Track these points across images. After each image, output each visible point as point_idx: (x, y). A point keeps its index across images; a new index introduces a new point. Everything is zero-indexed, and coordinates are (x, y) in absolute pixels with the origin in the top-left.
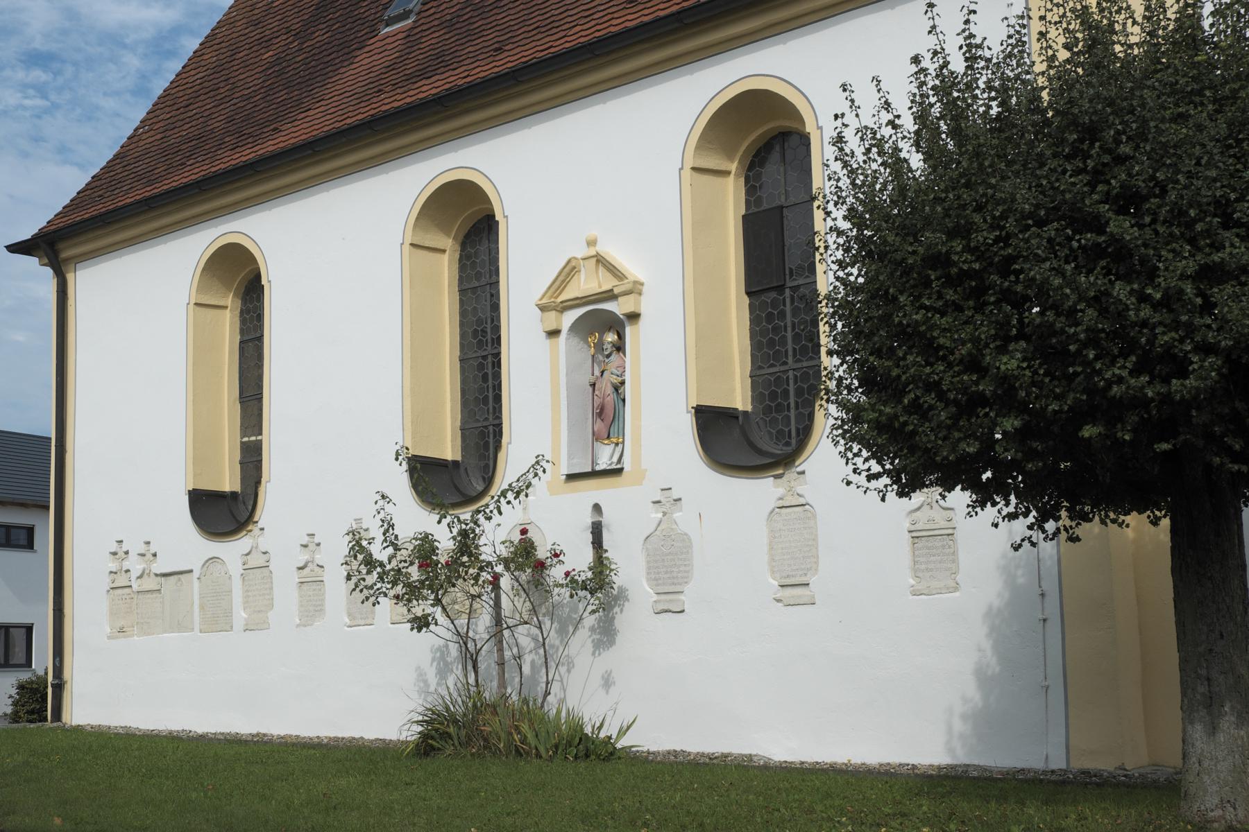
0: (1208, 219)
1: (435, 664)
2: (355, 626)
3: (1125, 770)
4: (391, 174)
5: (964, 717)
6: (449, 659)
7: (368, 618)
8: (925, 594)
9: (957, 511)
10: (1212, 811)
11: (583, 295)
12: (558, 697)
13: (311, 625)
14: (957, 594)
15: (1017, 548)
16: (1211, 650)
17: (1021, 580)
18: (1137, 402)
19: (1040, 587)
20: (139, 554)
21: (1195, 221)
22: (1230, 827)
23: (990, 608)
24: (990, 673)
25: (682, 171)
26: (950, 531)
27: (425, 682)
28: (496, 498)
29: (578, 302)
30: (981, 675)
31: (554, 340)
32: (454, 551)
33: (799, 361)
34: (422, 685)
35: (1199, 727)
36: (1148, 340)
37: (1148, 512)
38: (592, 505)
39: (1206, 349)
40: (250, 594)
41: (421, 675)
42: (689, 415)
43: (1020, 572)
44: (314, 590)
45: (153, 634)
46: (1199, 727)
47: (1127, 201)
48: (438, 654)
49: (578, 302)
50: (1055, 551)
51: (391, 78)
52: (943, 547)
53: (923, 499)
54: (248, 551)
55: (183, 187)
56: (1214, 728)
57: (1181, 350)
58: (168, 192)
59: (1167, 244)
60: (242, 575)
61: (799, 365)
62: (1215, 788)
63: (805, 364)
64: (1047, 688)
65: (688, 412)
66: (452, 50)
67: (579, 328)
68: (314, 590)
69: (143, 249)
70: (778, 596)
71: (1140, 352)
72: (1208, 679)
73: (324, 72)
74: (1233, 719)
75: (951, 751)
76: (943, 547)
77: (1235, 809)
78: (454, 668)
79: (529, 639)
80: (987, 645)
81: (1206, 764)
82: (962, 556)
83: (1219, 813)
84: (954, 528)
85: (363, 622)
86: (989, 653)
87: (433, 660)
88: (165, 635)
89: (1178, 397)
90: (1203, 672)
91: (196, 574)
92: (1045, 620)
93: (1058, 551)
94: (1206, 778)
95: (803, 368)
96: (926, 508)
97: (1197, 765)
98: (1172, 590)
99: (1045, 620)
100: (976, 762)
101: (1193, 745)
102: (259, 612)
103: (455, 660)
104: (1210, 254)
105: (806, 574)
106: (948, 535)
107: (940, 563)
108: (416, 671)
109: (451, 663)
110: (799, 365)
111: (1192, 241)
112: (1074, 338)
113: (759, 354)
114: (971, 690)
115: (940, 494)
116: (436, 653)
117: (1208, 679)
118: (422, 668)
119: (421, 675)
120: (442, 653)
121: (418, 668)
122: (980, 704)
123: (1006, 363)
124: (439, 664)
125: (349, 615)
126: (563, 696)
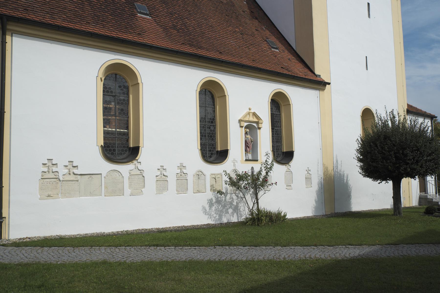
1: (209, 204)
2: (180, 194)
5: (314, 208)
12: (243, 210)
14: (311, 188)
20: (64, 166)
27: (205, 209)
28: (262, 163)
29: (248, 121)
31: (242, 128)
34: (204, 210)
38: (252, 167)
40: (132, 183)
42: (98, 147)
45: (73, 197)
49: (248, 121)
54: (140, 169)
55: (47, 24)
58: (71, 29)
60: (129, 177)
61: (276, 144)
63: (278, 144)
65: (270, 150)
66: (119, 26)
67: (247, 127)
73: (249, 51)
85: (182, 193)
86: (316, 197)
88: (80, 198)
91: (104, 175)
102: (137, 189)
103: (215, 202)
108: (202, 206)
109: (214, 203)
110: (276, 144)
113: (204, 137)
118: (204, 206)
119: (204, 208)
120: (211, 201)
122: (315, 205)
124: (210, 204)
125: (177, 191)
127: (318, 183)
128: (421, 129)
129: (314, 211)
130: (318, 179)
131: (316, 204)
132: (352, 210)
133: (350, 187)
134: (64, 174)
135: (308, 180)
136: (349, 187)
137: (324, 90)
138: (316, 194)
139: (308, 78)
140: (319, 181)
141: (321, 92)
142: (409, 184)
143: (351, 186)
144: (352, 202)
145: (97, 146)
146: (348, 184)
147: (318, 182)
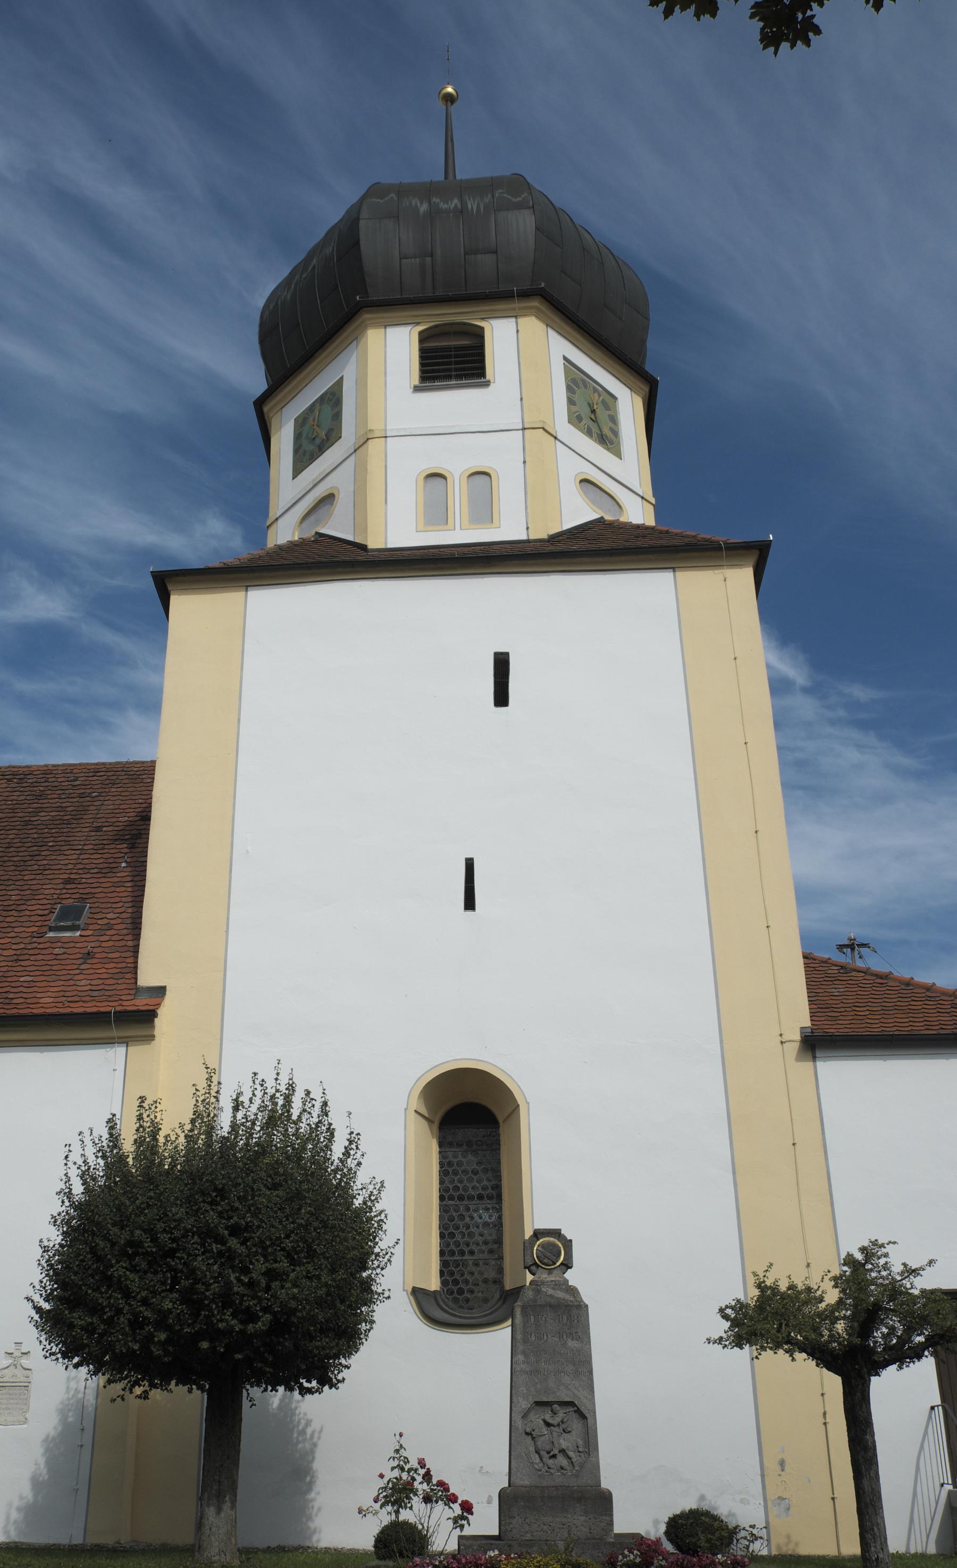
0: (275, 1247)
3: (121, 1544)
5: (19, 1509)
8: (3, 1425)
10: (214, 1556)
14: (25, 1426)
15: (113, 1400)
16: (222, 1465)
17: (71, 1419)
18: (229, 1331)
19: (82, 1424)
21: (267, 1247)
22: (223, 1566)
23: (48, 1437)
24: (41, 1479)
26: (27, 1384)
30: (36, 1483)
35: (212, 1509)
36: (239, 1302)
37: (189, 1386)
39: (265, 1310)
43: (71, 1414)
46: (212, 1509)
47: (235, 1231)
50: (95, 1402)
52: (20, 1394)
53: (11, 1361)
56: (219, 1509)
57: (255, 1309)
59: (254, 1256)
62: (217, 1543)
64: (77, 1490)
71: (234, 1307)
72: (219, 1482)
74: (230, 1505)
75: (6, 1532)
76: (20, 1394)
77: (225, 1555)
80: (42, 1461)
81: (213, 1529)
82: (32, 1402)
83: (217, 1558)
84: (30, 1382)
86: (42, 1466)
89: (249, 1332)
90: (217, 1478)
92: (82, 1446)
93: (96, 1403)
94: (213, 1538)
96: (12, 1367)
97: (208, 1530)
98: (846, 1433)
99: (82, 1446)
100: (26, 1541)
101: (208, 1519)
104: (272, 1264)
106: (25, 1386)
107: (16, 1404)
111: (265, 1256)
112: (206, 1298)
114: (26, 1490)
117: (219, 1482)
123: (167, 1305)
127: (60, 1407)
128: (122, 1159)
129: (15, 1522)
130: (68, 1388)
131: (36, 1496)
132: (319, 1541)
133: (309, 1431)
134: (827, 1415)
135: (11, 1392)
136: (303, 1432)
137: (152, 1037)
138: (42, 1450)
139: (88, 1010)
140: (68, 1399)
141: (135, 1050)
142: (825, 1424)
143: (315, 1426)
144: (316, 1505)
145: (404, 1290)
146: (293, 1414)
147: (62, 1403)
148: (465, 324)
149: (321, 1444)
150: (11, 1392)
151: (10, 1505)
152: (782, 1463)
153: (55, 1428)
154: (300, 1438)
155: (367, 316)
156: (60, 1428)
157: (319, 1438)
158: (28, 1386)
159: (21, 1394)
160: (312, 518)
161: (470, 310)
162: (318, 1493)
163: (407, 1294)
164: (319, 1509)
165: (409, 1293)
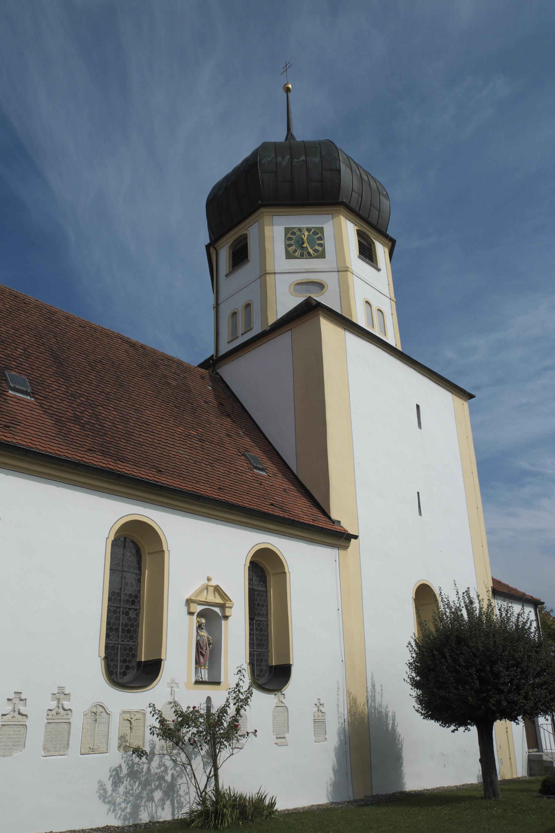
1: (111, 779)
4: (185, 518)
6: (121, 775)
7: (60, 751)
9: (326, 714)
11: (209, 602)
12: (185, 792)
13: (11, 755)
24: (336, 769)
25: (108, 539)
26: (323, 720)
27: (105, 790)
29: (205, 603)
30: (335, 772)
32: (182, 712)
33: (123, 641)
34: (102, 792)
41: (102, 786)
44: (15, 731)
48: (114, 773)
49: (205, 603)
51: (49, 433)
63: (260, 650)
67: (201, 614)
68: (15, 731)
69: (303, 543)
70: (276, 742)
75: (329, 800)
78: (125, 780)
79: (171, 762)
80: (335, 760)
85: (56, 753)
86: (335, 762)
87: (111, 776)
95: (258, 651)
103: (125, 775)
105: (284, 734)
109: (123, 777)
110: (257, 650)
114: (331, 775)
115: (167, 712)
116: (113, 772)
118: (102, 781)
119: (102, 786)
121: (100, 782)
124: (114, 778)
126: (188, 791)
130: (339, 722)
131: (335, 777)
138: (334, 754)
140: (340, 728)
148: (368, 236)
149: (404, 745)
150: (318, 724)
151: (327, 783)
152: (500, 747)
153: (337, 743)
154: (398, 743)
155: (342, 209)
156: (339, 742)
157: (403, 742)
158: (324, 722)
159: (322, 725)
160: (304, 287)
161: (371, 231)
162: (404, 767)
163: (101, 658)
164: (405, 774)
165: (102, 659)
